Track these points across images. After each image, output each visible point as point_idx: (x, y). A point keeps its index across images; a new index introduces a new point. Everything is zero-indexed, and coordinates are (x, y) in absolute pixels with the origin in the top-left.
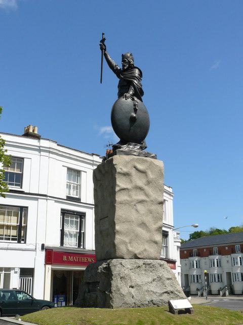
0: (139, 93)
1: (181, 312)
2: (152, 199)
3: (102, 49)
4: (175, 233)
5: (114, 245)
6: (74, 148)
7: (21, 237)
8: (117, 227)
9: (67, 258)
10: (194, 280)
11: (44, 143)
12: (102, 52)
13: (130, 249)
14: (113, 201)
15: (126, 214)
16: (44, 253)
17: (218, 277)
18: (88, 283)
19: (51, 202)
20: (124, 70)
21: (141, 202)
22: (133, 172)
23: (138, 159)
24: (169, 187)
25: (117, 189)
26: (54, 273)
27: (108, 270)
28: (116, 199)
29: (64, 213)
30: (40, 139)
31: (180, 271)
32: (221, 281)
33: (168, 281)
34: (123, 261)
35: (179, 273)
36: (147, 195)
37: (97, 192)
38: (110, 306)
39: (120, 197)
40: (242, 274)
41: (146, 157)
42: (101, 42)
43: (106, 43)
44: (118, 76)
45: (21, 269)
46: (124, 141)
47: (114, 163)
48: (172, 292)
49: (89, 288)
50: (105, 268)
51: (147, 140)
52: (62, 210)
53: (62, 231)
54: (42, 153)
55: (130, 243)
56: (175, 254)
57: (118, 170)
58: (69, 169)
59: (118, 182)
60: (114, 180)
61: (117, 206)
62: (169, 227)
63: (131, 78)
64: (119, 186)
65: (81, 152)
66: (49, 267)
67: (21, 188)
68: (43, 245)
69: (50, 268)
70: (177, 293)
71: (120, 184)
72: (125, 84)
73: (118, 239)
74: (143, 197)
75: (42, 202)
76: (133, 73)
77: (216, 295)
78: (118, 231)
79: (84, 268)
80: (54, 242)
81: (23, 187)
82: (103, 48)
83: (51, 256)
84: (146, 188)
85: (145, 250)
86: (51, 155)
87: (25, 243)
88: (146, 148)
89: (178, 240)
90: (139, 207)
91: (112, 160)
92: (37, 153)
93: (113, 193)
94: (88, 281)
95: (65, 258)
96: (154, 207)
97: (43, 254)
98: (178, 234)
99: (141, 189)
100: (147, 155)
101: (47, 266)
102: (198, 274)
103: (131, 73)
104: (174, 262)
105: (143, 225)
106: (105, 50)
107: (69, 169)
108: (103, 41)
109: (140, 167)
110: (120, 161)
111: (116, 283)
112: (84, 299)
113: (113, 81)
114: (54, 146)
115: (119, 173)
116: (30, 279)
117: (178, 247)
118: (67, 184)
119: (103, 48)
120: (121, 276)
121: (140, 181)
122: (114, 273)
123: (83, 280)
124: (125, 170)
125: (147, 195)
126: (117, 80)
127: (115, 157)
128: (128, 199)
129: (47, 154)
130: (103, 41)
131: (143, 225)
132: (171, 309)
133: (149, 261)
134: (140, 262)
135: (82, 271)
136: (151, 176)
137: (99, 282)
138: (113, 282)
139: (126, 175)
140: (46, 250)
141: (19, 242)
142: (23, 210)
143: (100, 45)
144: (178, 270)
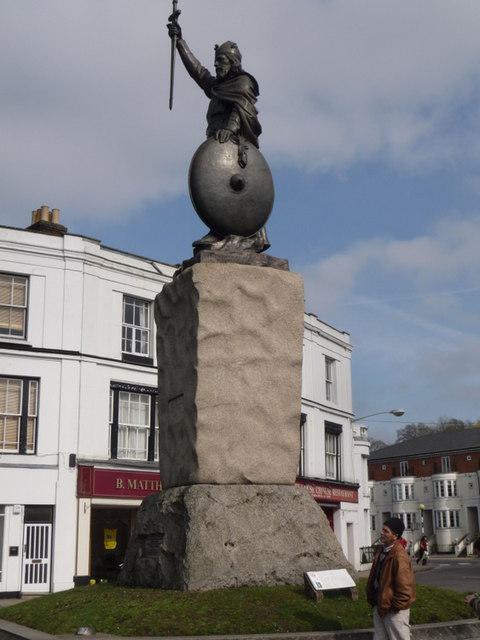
0: (250, 132)
1: (331, 594)
2: (277, 355)
3: (171, 34)
4: (357, 428)
5: (194, 456)
6: (9, 225)
7: (25, 443)
8: (202, 417)
9: (126, 483)
10: (445, 521)
11: (72, 243)
12: (173, 41)
13: (230, 462)
14: (194, 361)
15: (217, 384)
16: (75, 472)
17: (452, 517)
18: (143, 537)
19: (89, 366)
20: (220, 80)
21: (254, 362)
22: (236, 297)
23: (247, 270)
24: (343, 333)
25: (201, 334)
26: (97, 513)
27: (180, 505)
28: (200, 356)
29: (118, 388)
30: (62, 236)
31: (368, 506)
32: (458, 525)
33: (311, 531)
34: (214, 490)
35: (366, 510)
36: (266, 347)
37: (163, 341)
38: (326, 422)
39: (205, 353)
40: (473, 510)
41: (266, 265)
42: (170, 19)
43: (180, 21)
44: (209, 94)
45: (26, 506)
46: (219, 230)
47: (194, 279)
48: (318, 554)
49: (144, 549)
50: (174, 504)
51: (270, 231)
52: (112, 383)
53: (115, 428)
54: (70, 264)
55: (230, 449)
56: (355, 469)
57: (203, 294)
58: (128, 298)
59: (202, 321)
60: (195, 315)
61: (201, 371)
62: (342, 414)
63: (233, 97)
64: (205, 329)
65: (126, 254)
66: (87, 502)
67: (26, 339)
68: (73, 457)
69: (88, 504)
70: (328, 555)
71: (208, 326)
72: (220, 109)
73: (203, 442)
74: (256, 352)
75: (70, 364)
76: (238, 85)
77: (447, 553)
78: (202, 425)
79: (138, 503)
80: (96, 449)
81: (28, 339)
82: (174, 31)
83: (91, 480)
84: (264, 332)
85: (262, 464)
86: (88, 268)
87: (35, 453)
88: (266, 247)
89: (364, 443)
90: (249, 372)
91: (190, 273)
92: (60, 263)
93: (192, 345)
94: (143, 532)
95: (120, 483)
96: (282, 373)
97: (72, 475)
98: (363, 429)
99: (253, 334)
100: (269, 262)
101: (81, 500)
102: (409, 511)
103: (234, 86)
104: (354, 487)
105: (258, 410)
106: (179, 35)
107: (128, 298)
108: (176, 14)
109: (252, 287)
110: (210, 278)
111: (198, 533)
112: (134, 570)
113: (196, 103)
114: (94, 248)
115: (206, 301)
116: (47, 528)
117: (364, 456)
118: (124, 328)
119: (174, 31)
120: (208, 519)
121: (252, 319)
122: (193, 514)
123: (141, 526)
124: (218, 293)
125: (266, 347)
126: (204, 102)
127: (196, 267)
128: (225, 356)
129: (79, 265)
130: (176, 14)
131: (258, 410)
132: (307, 589)
133: (269, 489)
134: (252, 491)
135: (136, 509)
136: (275, 306)
137: (163, 534)
138: (189, 535)
139: (221, 304)
140: (79, 467)
141: (22, 452)
142: (30, 382)
143: (168, 26)
144: (364, 502)
